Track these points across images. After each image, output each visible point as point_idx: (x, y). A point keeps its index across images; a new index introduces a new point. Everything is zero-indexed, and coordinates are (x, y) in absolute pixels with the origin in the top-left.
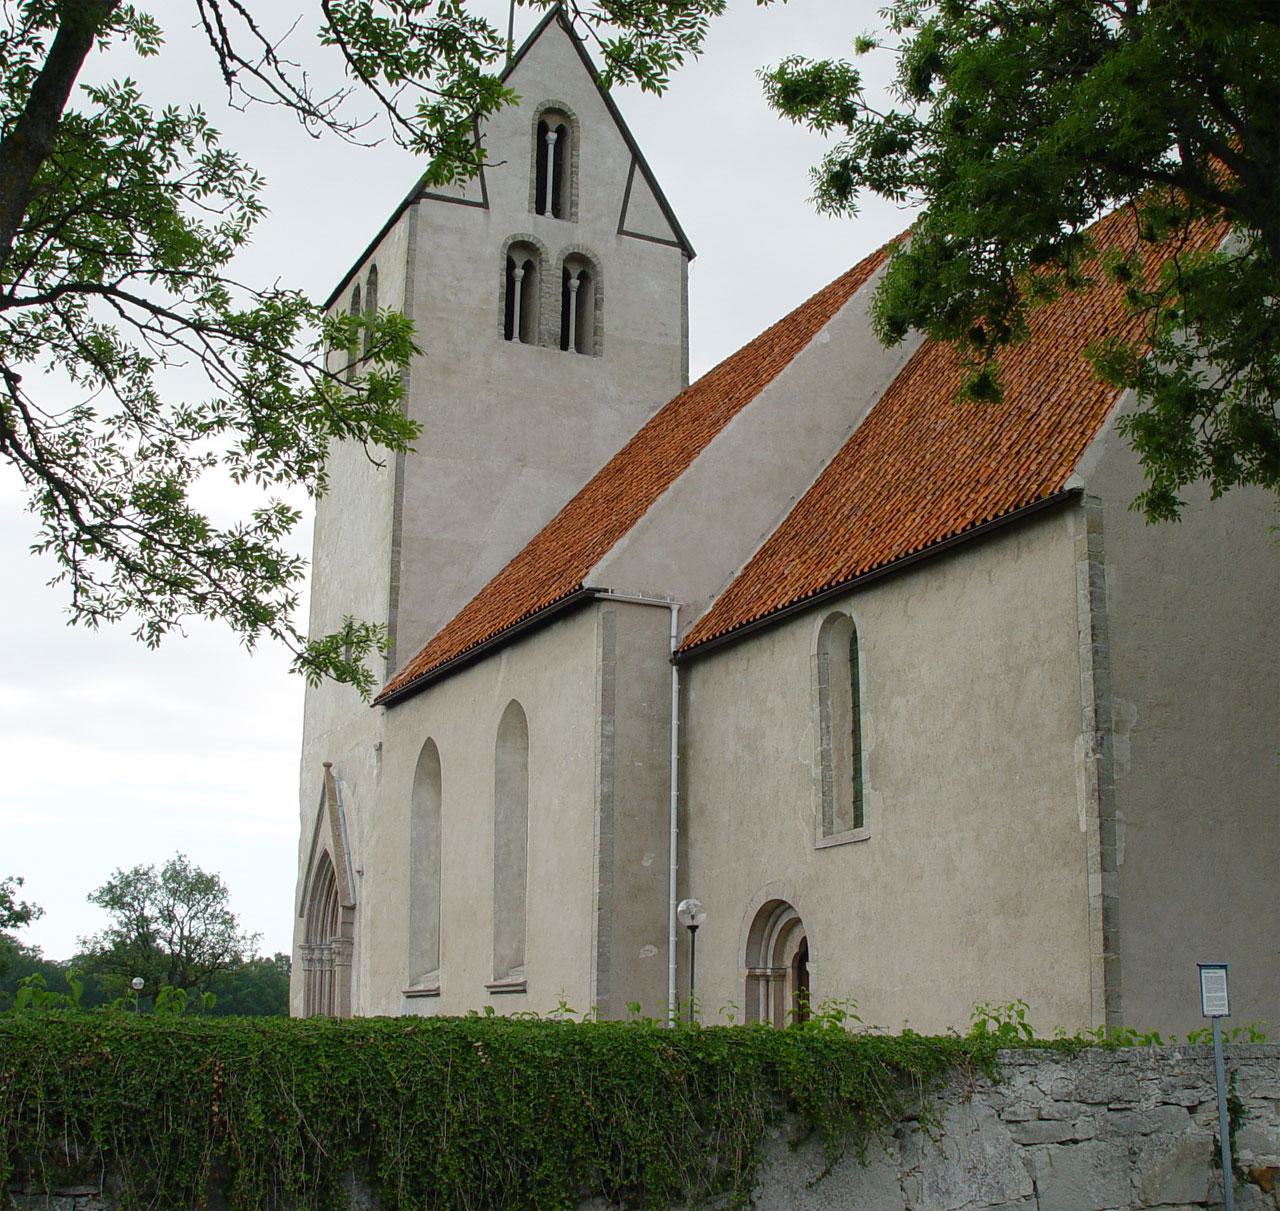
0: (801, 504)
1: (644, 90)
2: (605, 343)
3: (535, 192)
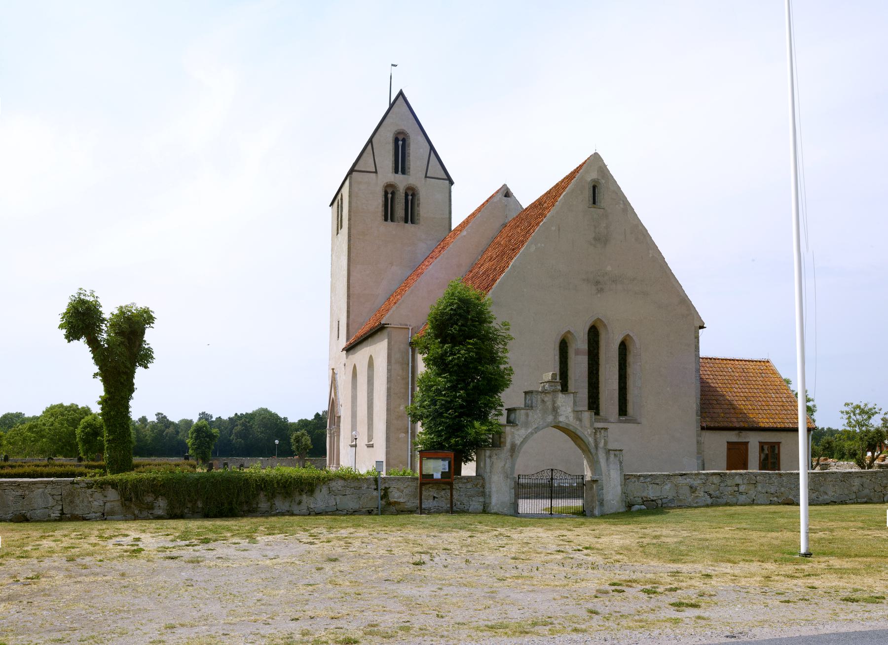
2: (421, 219)
3: (394, 165)
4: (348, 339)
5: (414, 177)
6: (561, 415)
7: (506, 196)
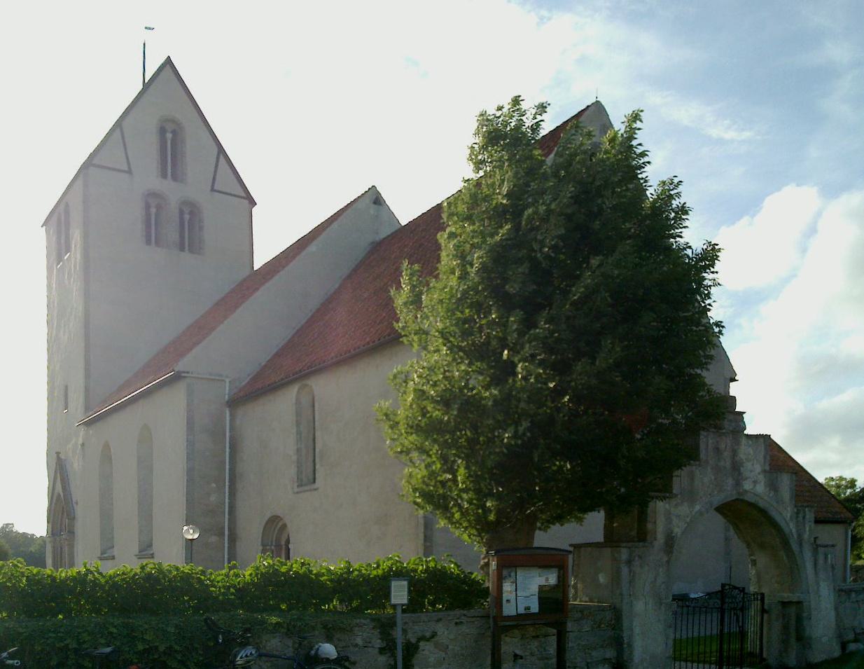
0: (298, 331)
3: (160, 166)
4: (87, 408)
5: (195, 187)
6: (746, 479)
7: (375, 203)
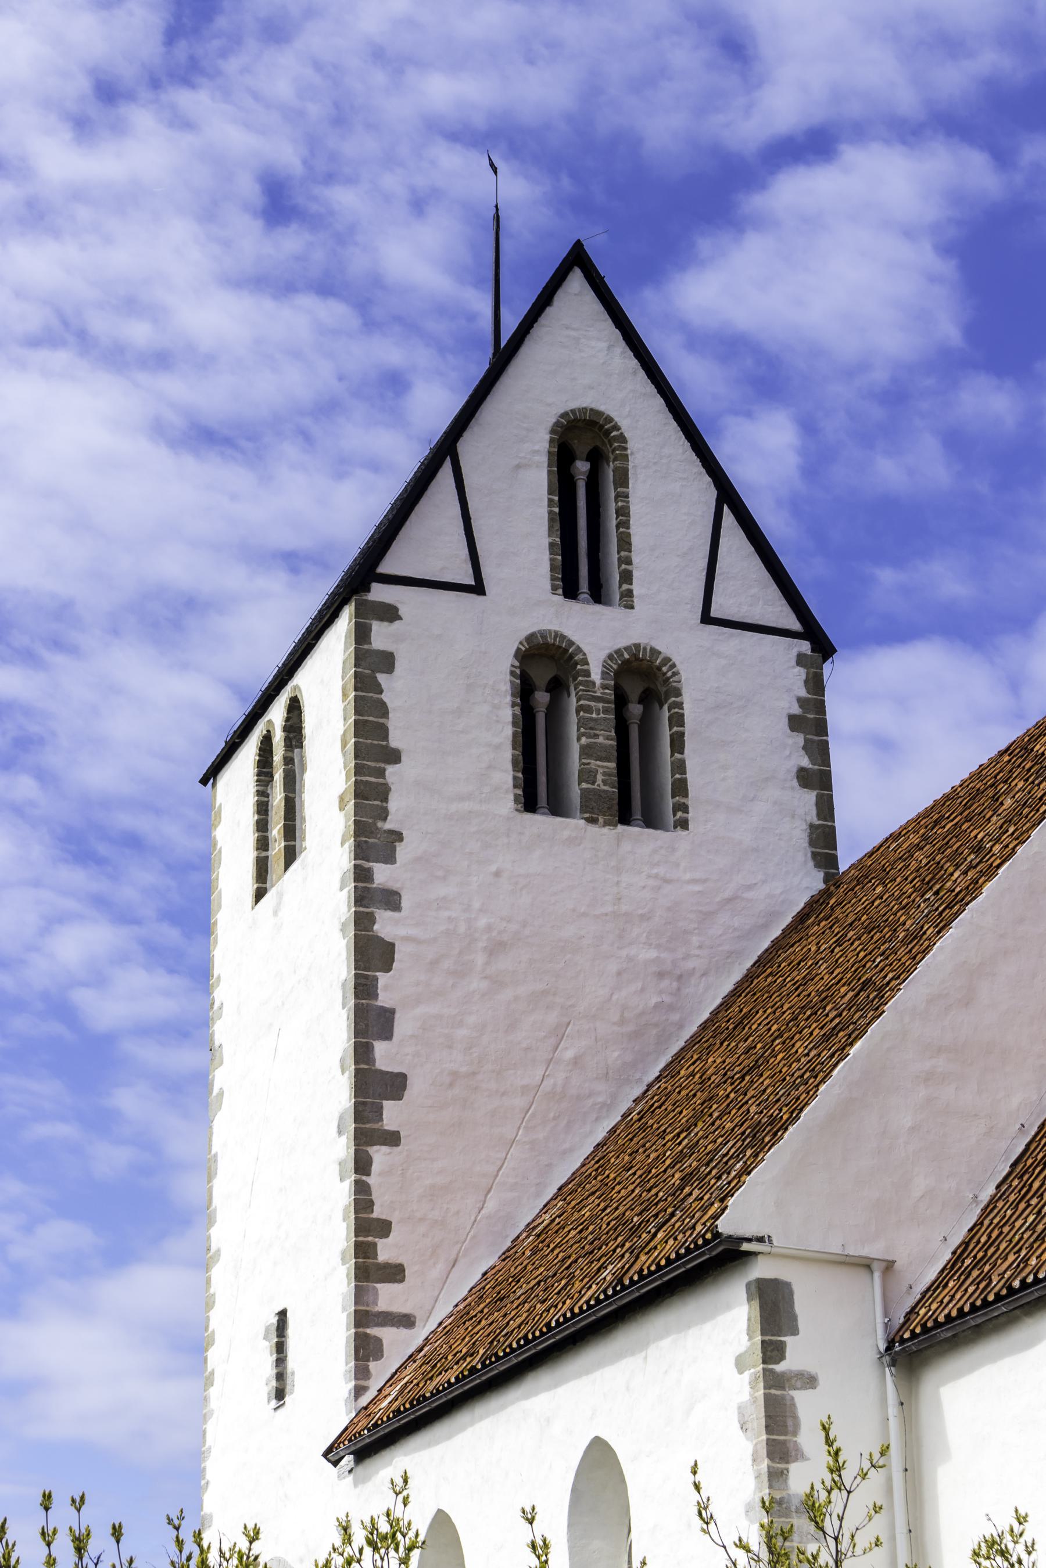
1: (1027, 1515)
